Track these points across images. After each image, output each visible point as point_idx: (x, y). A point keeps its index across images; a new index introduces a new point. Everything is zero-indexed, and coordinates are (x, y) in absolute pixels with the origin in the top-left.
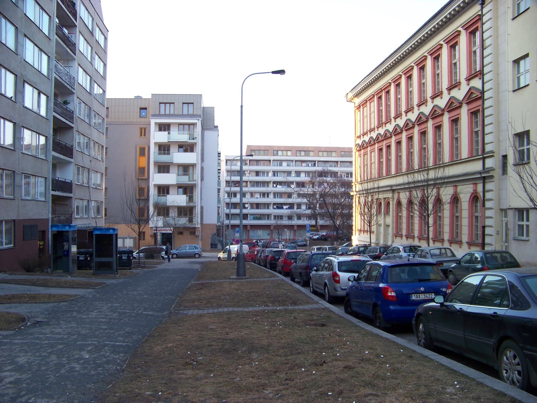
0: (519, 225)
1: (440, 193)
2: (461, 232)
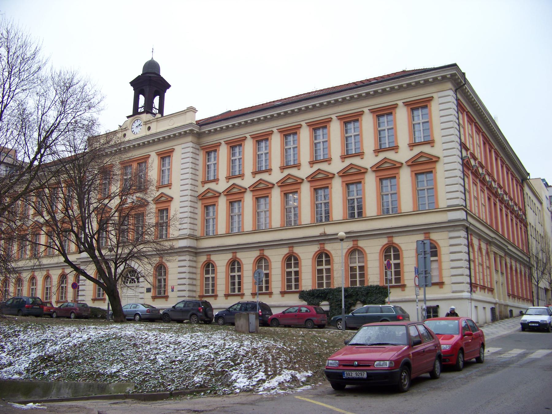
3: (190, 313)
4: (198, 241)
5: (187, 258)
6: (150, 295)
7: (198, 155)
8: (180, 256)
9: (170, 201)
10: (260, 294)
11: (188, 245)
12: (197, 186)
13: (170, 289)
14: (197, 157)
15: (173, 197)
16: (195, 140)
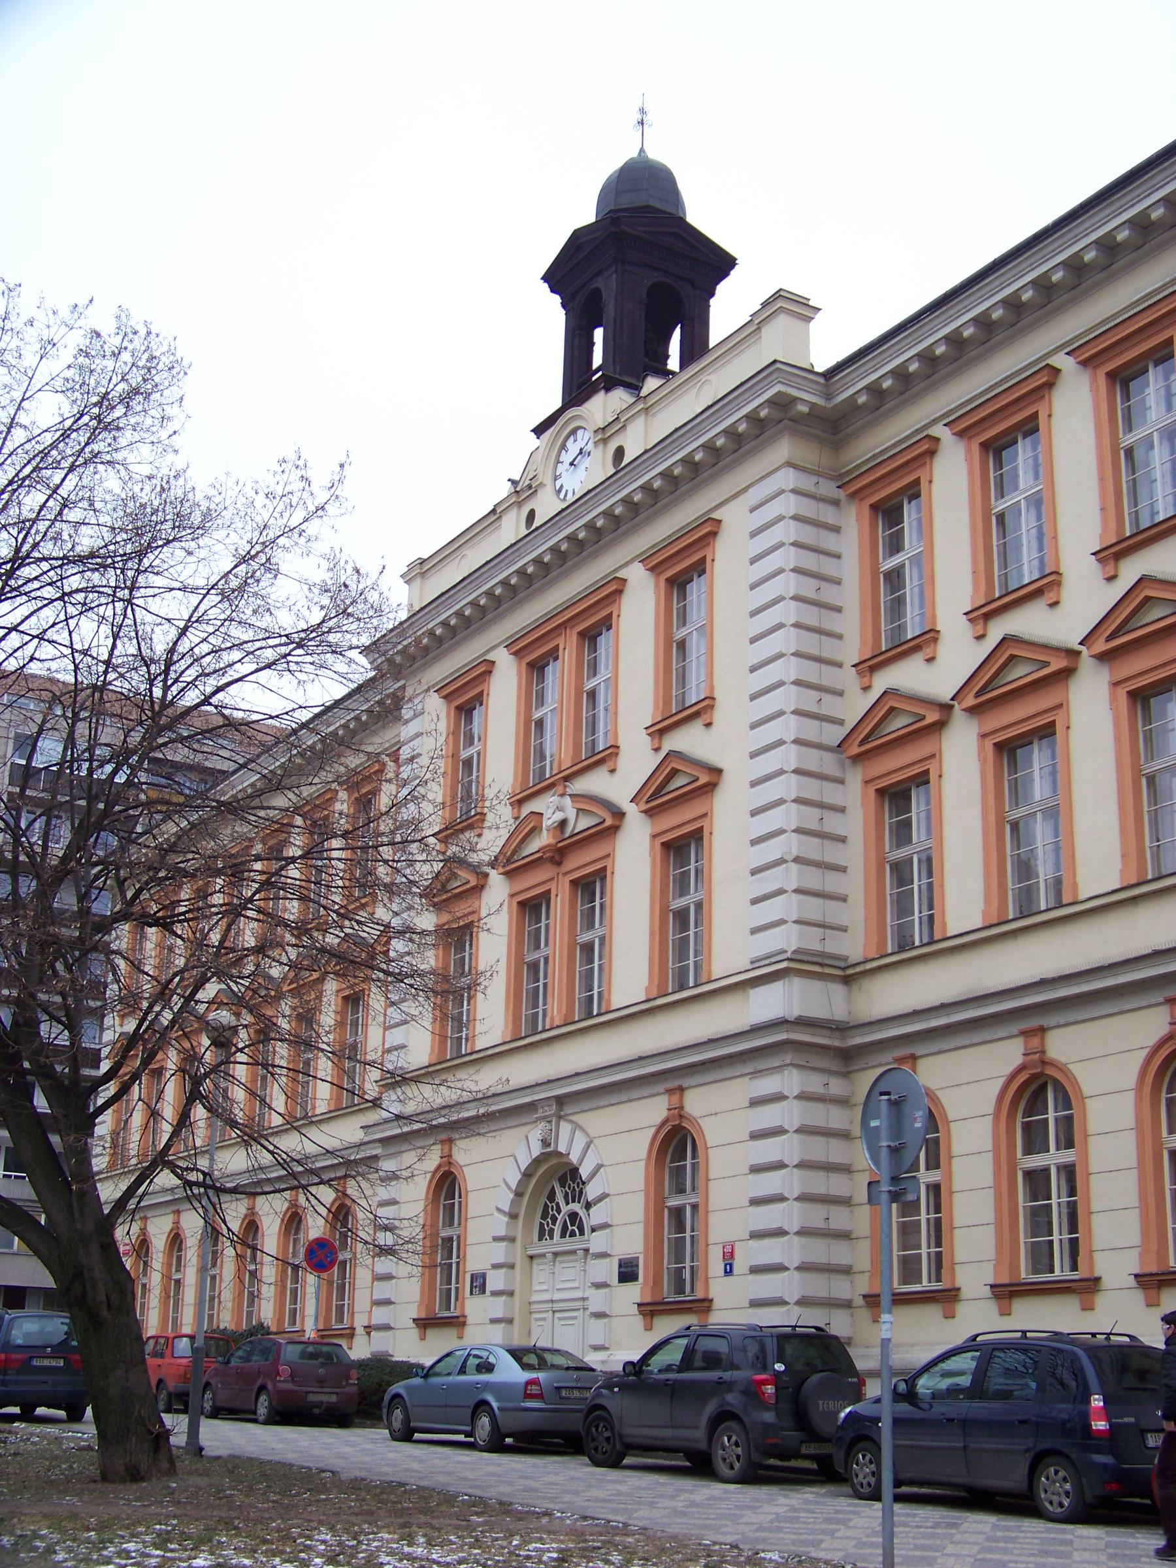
0: (1028, 1174)
1: (257, 1209)
2: (352, 1306)
3: (711, 1408)
4: (855, 988)
5: (790, 1081)
6: (633, 1292)
7: (836, 530)
8: (756, 1074)
9: (710, 787)
10: (900, 1300)
11: (795, 1012)
12: (840, 694)
13: (716, 1266)
14: (830, 542)
15: (720, 765)
16: (809, 454)
